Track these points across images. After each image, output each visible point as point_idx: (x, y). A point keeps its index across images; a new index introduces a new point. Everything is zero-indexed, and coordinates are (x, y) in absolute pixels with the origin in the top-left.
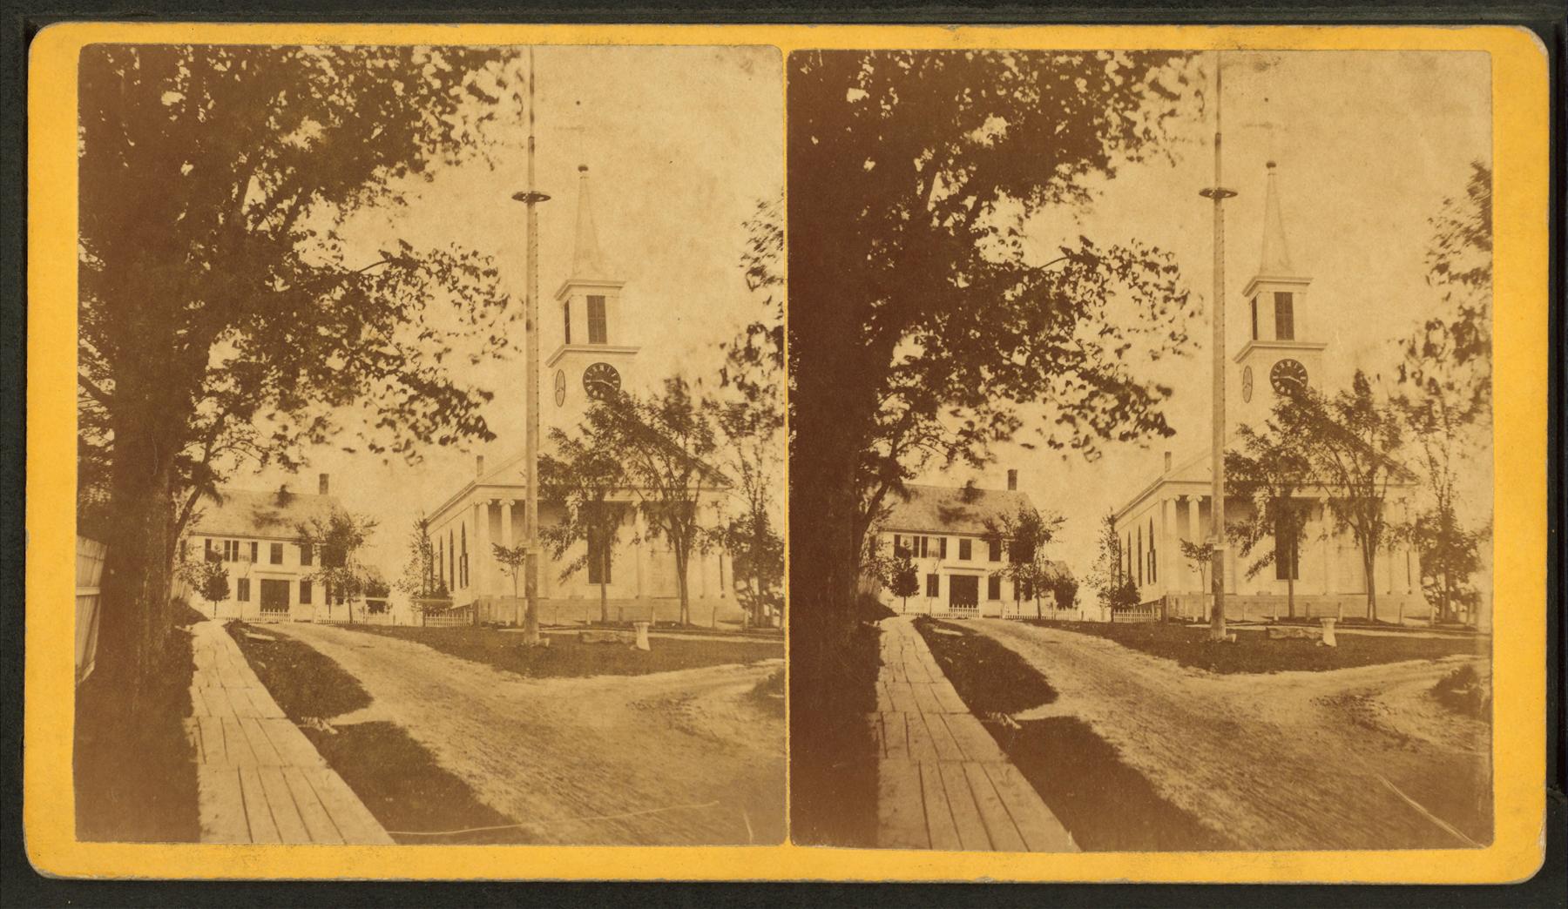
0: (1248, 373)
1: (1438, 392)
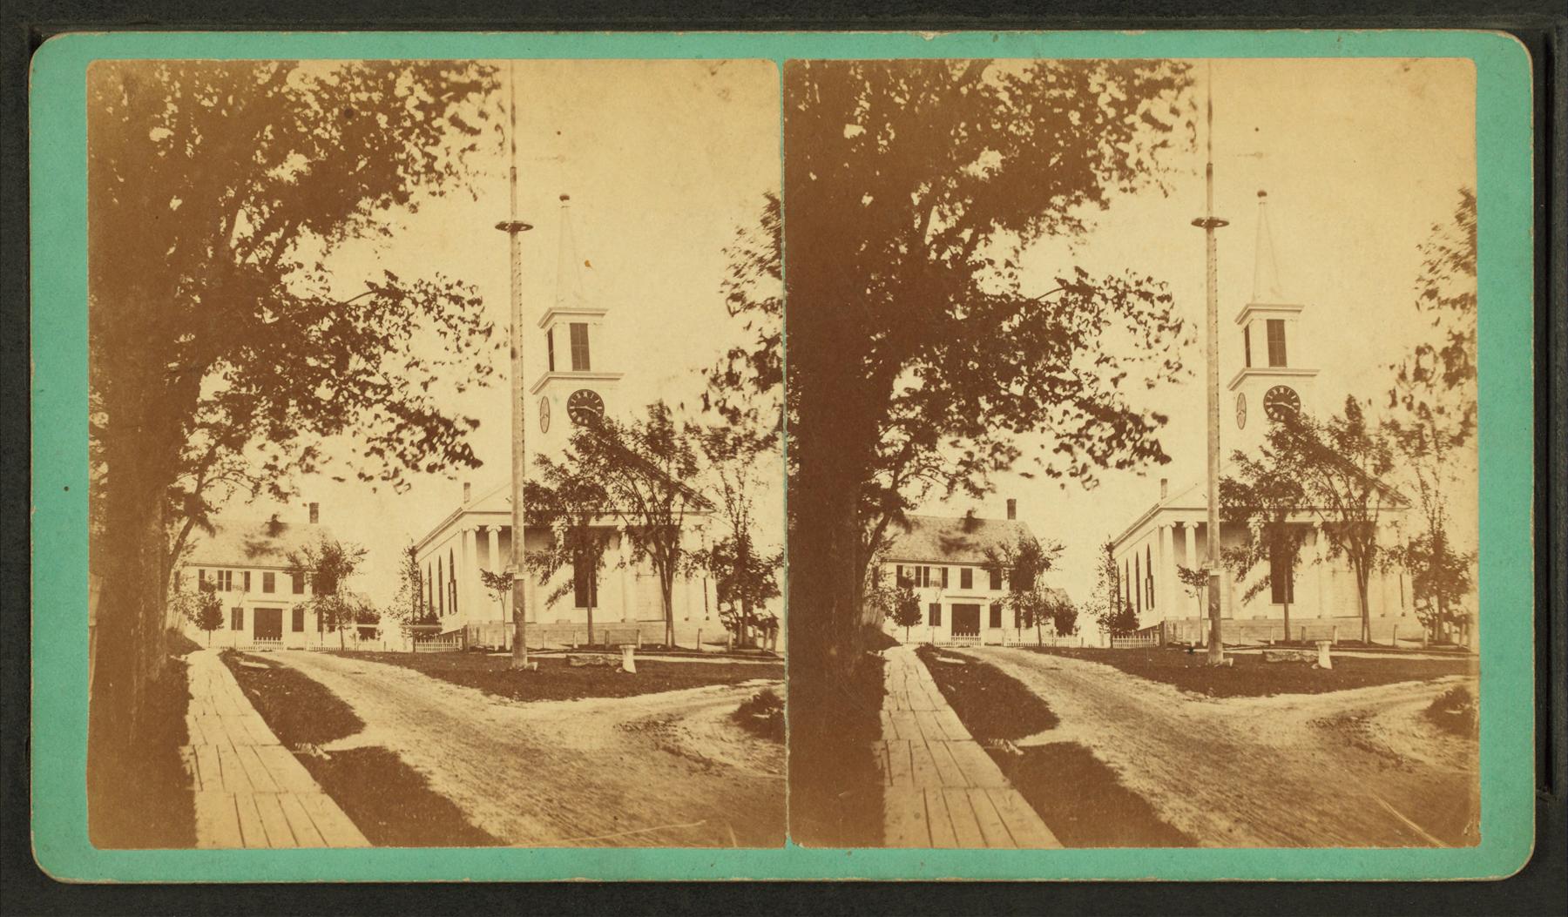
0: (1241, 399)
1: (1428, 416)
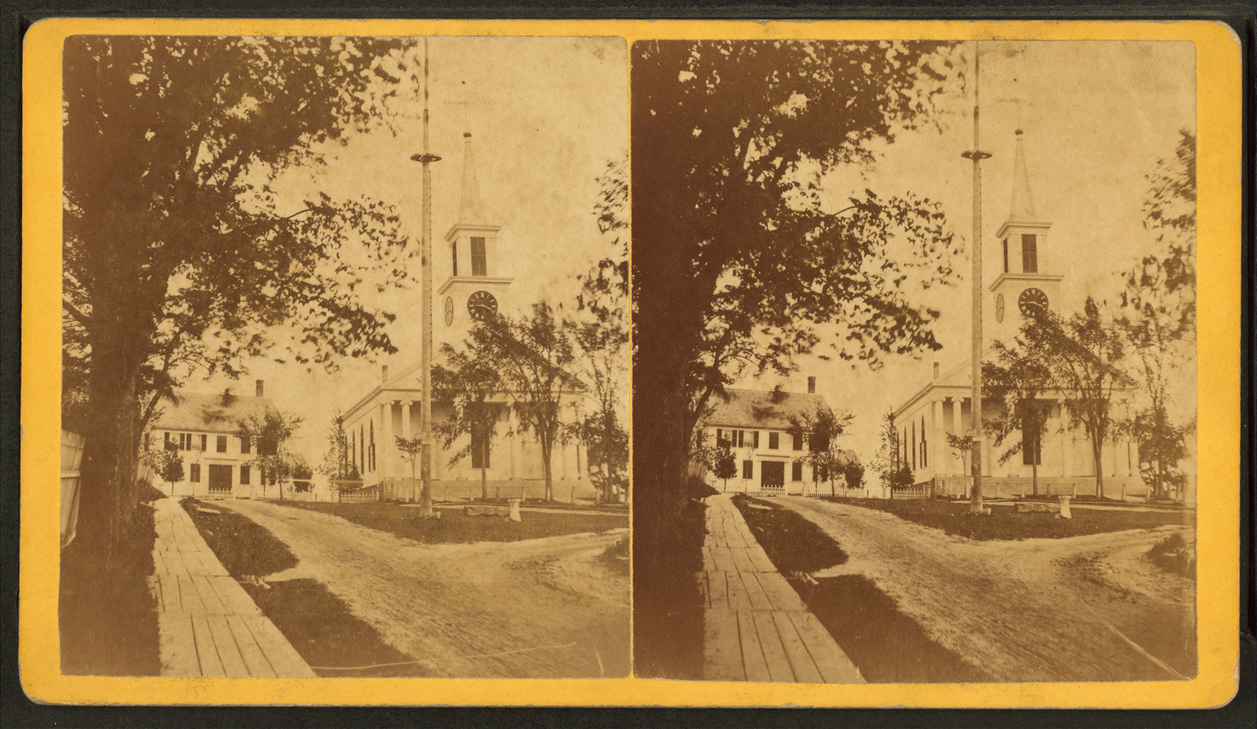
0: (1000, 299)
1: (1153, 315)
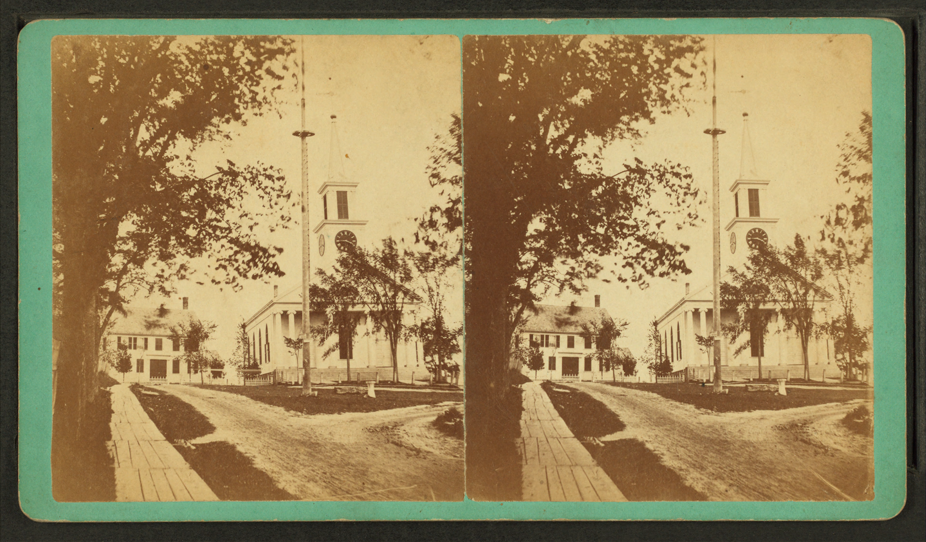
1: (844, 246)
